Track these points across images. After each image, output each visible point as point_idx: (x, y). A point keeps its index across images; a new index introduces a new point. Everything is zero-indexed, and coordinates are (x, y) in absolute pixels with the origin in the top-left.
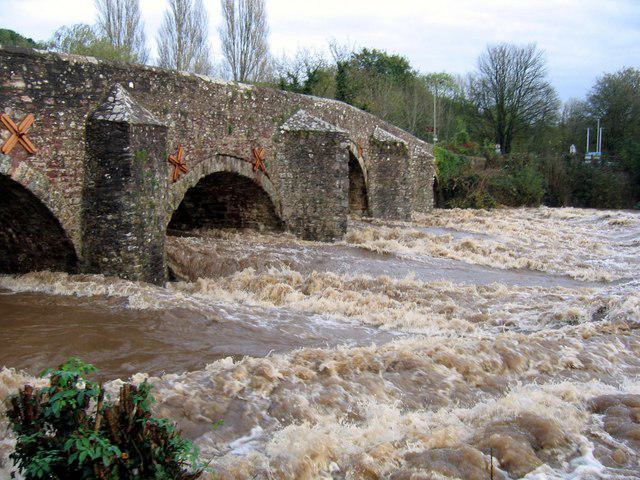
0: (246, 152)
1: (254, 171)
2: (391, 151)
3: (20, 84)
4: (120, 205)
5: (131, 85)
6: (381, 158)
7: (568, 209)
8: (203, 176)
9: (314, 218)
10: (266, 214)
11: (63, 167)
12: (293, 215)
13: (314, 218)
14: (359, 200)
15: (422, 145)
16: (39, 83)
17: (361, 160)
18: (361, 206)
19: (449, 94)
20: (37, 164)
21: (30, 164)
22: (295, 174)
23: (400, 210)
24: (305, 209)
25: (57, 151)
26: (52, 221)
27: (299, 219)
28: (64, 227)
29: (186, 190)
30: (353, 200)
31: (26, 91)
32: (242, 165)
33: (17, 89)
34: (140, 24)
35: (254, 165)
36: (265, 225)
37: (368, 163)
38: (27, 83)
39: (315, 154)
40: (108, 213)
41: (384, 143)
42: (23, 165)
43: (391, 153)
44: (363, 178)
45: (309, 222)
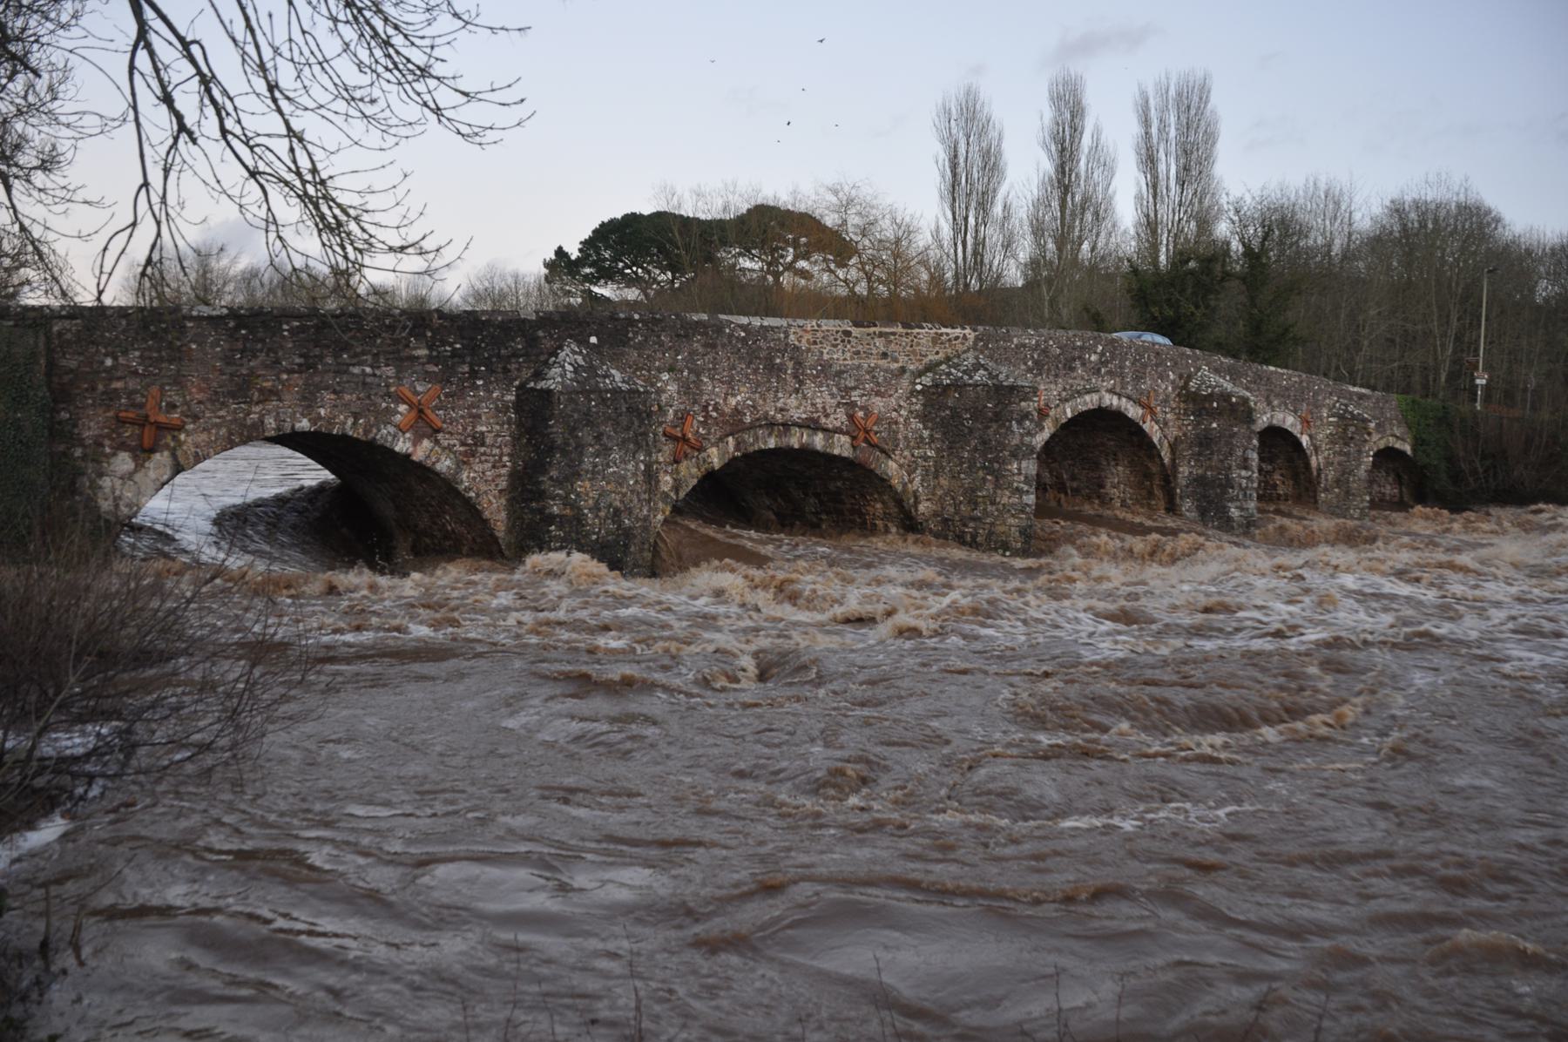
0: (839, 418)
3: (423, 352)
4: (544, 492)
5: (593, 340)
6: (1199, 424)
7: (154, 917)
9: (974, 519)
10: (894, 510)
11: (483, 445)
12: (936, 514)
14: (1158, 492)
16: (448, 348)
17: (1152, 429)
18: (1162, 504)
20: (445, 443)
21: (437, 442)
22: (938, 451)
23: (1234, 512)
24: (957, 506)
25: (474, 427)
26: (471, 510)
27: (947, 520)
28: (487, 514)
31: (431, 360)
33: (418, 358)
35: (854, 438)
37: (1173, 432)
38: (430, 348)
39: (961, 417)
40: (531, 500)
41: (1210, 397)
42: (426, 443)
43: (1220, 414)
45: (965, 525)
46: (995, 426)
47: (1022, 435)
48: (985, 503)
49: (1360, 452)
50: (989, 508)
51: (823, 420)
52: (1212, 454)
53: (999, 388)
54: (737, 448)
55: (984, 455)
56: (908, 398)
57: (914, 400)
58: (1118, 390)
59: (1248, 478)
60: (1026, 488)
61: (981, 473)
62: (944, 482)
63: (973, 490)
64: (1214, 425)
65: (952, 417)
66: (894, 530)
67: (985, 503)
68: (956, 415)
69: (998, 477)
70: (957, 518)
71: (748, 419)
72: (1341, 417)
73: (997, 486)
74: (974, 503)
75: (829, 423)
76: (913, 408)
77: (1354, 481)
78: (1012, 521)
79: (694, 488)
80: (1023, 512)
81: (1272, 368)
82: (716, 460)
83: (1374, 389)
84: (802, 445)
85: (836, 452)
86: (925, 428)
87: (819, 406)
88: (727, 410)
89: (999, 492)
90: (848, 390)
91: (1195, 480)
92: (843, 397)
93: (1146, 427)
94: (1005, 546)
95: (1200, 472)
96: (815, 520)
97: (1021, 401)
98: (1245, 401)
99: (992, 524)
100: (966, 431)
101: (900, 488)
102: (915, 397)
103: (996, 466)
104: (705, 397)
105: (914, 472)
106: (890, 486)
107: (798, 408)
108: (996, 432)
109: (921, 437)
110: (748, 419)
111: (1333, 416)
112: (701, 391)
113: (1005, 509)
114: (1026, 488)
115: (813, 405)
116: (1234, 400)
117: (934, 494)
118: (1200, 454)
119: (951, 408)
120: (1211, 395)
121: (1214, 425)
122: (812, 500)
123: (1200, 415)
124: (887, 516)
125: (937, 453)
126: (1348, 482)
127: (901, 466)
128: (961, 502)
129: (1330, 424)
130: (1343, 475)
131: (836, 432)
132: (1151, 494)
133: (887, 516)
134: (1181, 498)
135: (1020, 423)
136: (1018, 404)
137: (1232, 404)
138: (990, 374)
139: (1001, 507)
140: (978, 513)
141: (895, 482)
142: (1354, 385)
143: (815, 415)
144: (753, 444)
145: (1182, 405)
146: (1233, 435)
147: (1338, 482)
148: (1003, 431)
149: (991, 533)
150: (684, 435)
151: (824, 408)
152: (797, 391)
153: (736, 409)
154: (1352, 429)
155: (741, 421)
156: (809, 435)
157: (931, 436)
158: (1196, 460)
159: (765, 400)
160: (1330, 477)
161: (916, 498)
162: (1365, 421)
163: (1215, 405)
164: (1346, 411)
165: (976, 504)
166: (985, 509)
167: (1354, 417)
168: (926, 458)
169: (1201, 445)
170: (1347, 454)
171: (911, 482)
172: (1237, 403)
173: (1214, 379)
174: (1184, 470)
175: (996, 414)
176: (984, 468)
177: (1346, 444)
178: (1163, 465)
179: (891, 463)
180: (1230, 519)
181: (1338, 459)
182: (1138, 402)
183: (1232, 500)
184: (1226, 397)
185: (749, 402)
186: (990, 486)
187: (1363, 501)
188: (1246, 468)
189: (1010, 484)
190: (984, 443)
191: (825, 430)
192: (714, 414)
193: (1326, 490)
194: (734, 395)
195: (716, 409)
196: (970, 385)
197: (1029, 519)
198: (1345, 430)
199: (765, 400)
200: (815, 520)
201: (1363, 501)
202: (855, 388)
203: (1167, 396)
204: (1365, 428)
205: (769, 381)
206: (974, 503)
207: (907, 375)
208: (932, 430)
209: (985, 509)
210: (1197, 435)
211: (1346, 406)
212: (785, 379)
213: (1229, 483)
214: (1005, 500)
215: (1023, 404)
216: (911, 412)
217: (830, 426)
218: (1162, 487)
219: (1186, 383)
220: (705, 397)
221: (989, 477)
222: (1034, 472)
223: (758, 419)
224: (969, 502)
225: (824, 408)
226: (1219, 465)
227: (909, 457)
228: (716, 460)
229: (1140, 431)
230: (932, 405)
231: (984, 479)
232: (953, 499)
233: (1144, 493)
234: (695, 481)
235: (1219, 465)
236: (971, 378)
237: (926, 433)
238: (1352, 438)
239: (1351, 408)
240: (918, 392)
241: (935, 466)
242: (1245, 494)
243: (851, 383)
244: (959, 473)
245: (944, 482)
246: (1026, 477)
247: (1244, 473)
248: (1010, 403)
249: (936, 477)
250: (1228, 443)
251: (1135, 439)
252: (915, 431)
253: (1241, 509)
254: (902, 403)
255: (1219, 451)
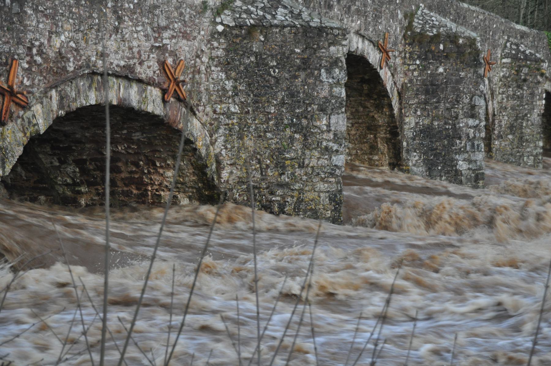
1: (164, 101)
2: (446, 56)
6: (425, 68)
8: (62, 113)
9: (281, 185)
10: (191, 178)
12: (241, 182)
13: (281, 185)
14: (382, 146)
15: (523, 35)
17: (385, 74)
18: (386, 160)
19: (9, 323)
22: (242, 105)
23: (462, 166)
24: (262, 171)
29: (25, 140)
30: (536, 269)
32: (142, 92)
34: (481, 246)
35: (164, 92)
36: (190, 198)
37: (401, 79)
39: (267, 65)
41: (436, 39)
43: (447, 57)
44: (390, 106)
45: (272, 193)
46: (302, 75)
47: (331, 86)
48: (293, 166)
49: (532, 94)
50: (298, 172)
51: (138, 69)
52: (438, 102)
53: (307, 29)
54: (61, 106)
55: (291, 110)
56: (209, 41)
57: (216, 44)
58: (362, 32)
59: (475, 127)
60: (335, 147)
61: (288, 132)
62: (249, 142)
63: (281, 151)
64: (441, 70)
65: (258, 64)
66: (185, 201)
67: (293, 166)
68: (261, 62)
69: (306, 133)
70: (264, 185)
71: (71, 67)
72: (515, 58)
73: (306, 146)
74: (281, 166)
75: (143, 72)
76: (215, 53)
77: (527, 126)
78: (322, 186)
79: (20, 158)
80: (332, 174)
81: (466, 5)
82: (41, 121)
83: (532, 26)
84: (120, 100)
85: (150, 109)
86: (228, 78)
87: (135, 50)
88: (52, 55)
89: (307, 152)
90: (160, 30)
91: (421, 131)
92: (156, 39)
93: (382, 73)
94: (315, 215)
95: (427, 122)
96: (69, 193)
97: (330, 44)
98: (472, 42)
99: (301, 191)
100: (273, 81)
101: (203, 152)
102: (217, 40)
103: (304, 122)
104: (30, 36)
105: (217, 131)
106: (195, 149)
107: (116, 52)
108: (305, 83)
109: (224, 89)
110: (71, 67)
111: (506, 57)
112: (26, 26)
113: (314, 172)
114: (335, 147)
115: (130, 48)
116: (461, 41)
117: (239, 158)
118: (426, 103)
119: (256, 55)
120: (438, 36)
121: (441, 70)
122: (70, 169)
123: (426, 59)
124: (180, 186)
125: (242, 108)
126: (521, 127)
127: (204, 125)
128: (268, 166)
129: (503, 65)
130: (516, 120)
131: (149, 84)
132: (373, 148)
133: (180, 186)
134: (408, 151)
135: (329, 71)
136: (327, 49)
137: (458, 46)
138: (291, 12)
139: (309, 170)
140: (285, 178)
141: (199, 144)
142: (517, 23)
143: (132, 62)
144: (75, 100)
145: (408, 48)
146: (460, 81)
147: (511, 127)
148: (311, 81)
149: (300, 201)
150: (11, 87)
151: (139, 52)
152: (116, 30)
153: (60, 53)
154: (525, 70)
155: (64, 69)
156: (126, 88)
157: (235, 87)
158: (424, 109)
159: (87, 42)
160: (503, 123)
161: (218, 162)
162: (538, 61)
163: (441, 47)
164: (518, 50)
165: (284, 167)
166: (293, 174)
167: (526, 58)
168: (229, 115)
169: (427, 92)
170: (520, 98)
171: (213, 143)
172: (465, 45)
173: (436, 18)
174: (410, 121)
175: (305, 61)
176: (292, 125)
177: (519, 87)
178: (392, 116)
179: (195, 121)
180: (458, 173)
181: (511, 103)
182: (377, 45)
183: (459, 152)
184: (452, 38)
185: (72, 44)
186: (298, 146)
187: (536, 147)
188: (473, 116)
189: (319, 143)
190: (292, 95)
191: (140, 81)
192: (38, 59)
193: (500, 137)
194: (58, 34)
195: (40, 53)
196: (276, 26)
197: (338, 183)
198: (518, 72)
199: (87, 42)
200: (69, 193)
201: (536, 147)
202: (166, 28)
203: (396, 38)
204: (538, 69)
205: (91, 17)
206: (281, 166)
207: (208, 13)
208: (236, 80)
209: (293, 174)
210: (423, 82)
211: (517, 45)
212: (105, 14)
213: (457, 134)
214: (314, 162)
215: (332, 48)
216: (211, 58)
217: (143, 76)
218: (388, 141)
219: (410, 23)
220: (30, 36)
221: (297, 136)
222: (344, 129)
223: (81, 67)
224: (276, 166)
225: (139, 52)
226: (446, 114)
227: (211, 113)
228: (41, 121)
229: (377, 76)
230: (235, 51)
231: (292, 138)
232: (259, 162)
233: (366, 147)
234: (19, 151)
235: (446, 114)
236: (274, 17)
237: (229, 85)
238: (525, 80)
239: (522, 48)
240: (220, 34)
241: (239, 124)
242: (473, 146)
243: (163, 23)
244: (265, 132)
245: (249, 142)
246: (335, 135)
247: (471, 122)
248: (319, 48)
249: (241, 138)
250: (456, 90)
251: (366, 87)
252: (217, 82)
253: (470, 161)
254: (204, 48)
255: (446, 98)
